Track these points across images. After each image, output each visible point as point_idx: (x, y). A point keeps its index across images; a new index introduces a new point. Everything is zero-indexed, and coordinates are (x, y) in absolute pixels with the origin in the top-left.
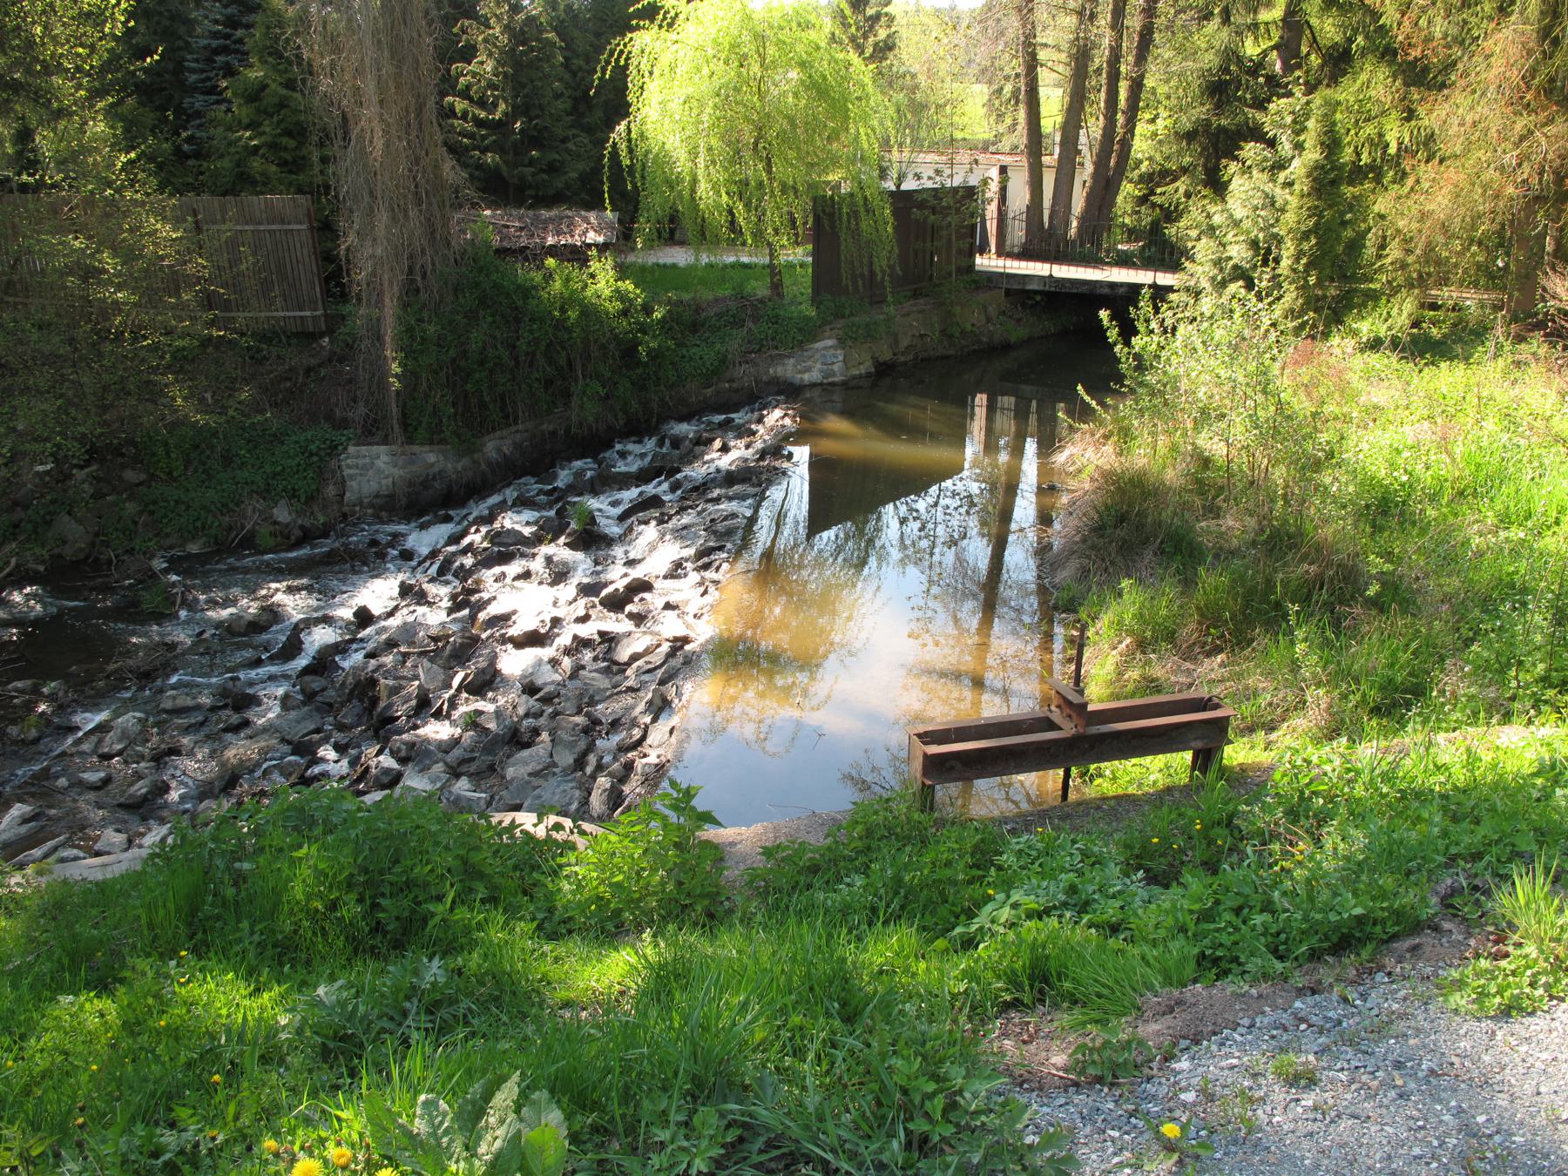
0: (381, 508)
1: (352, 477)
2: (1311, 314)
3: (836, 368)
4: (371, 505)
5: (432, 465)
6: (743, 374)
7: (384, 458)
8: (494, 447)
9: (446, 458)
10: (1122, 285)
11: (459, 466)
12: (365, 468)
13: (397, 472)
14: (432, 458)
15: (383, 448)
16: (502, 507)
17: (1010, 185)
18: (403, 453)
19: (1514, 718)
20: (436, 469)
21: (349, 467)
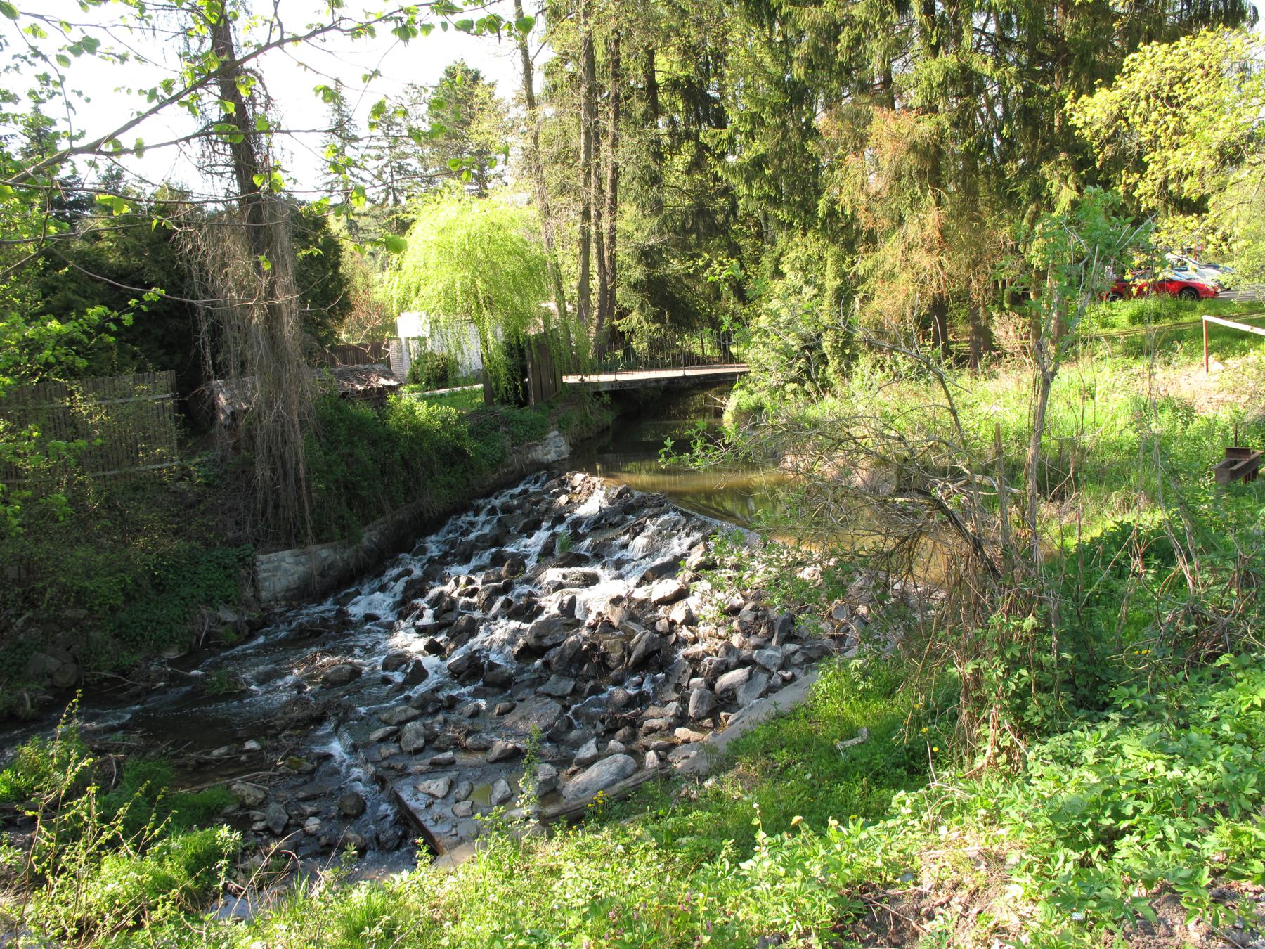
0: (293, 598)
1: (265, 579)
2: (17, 200)
3: (563, 448)
4: (285, 598)
5: (325, 559)
6: (515, 461)
7: (290, 560)
8: (370, 536)
9: (335, 551)
10: (664, 379)
11: (345, 556)
12: (276, 569)
13: (301, 569)
14: (324, 553)
15: (287, 552)
16: (435, 571)
17: (519, 81)
18: (303, 554)
19: (1215, 448)
20: (329, 561)
21: (265, 571)
